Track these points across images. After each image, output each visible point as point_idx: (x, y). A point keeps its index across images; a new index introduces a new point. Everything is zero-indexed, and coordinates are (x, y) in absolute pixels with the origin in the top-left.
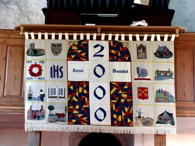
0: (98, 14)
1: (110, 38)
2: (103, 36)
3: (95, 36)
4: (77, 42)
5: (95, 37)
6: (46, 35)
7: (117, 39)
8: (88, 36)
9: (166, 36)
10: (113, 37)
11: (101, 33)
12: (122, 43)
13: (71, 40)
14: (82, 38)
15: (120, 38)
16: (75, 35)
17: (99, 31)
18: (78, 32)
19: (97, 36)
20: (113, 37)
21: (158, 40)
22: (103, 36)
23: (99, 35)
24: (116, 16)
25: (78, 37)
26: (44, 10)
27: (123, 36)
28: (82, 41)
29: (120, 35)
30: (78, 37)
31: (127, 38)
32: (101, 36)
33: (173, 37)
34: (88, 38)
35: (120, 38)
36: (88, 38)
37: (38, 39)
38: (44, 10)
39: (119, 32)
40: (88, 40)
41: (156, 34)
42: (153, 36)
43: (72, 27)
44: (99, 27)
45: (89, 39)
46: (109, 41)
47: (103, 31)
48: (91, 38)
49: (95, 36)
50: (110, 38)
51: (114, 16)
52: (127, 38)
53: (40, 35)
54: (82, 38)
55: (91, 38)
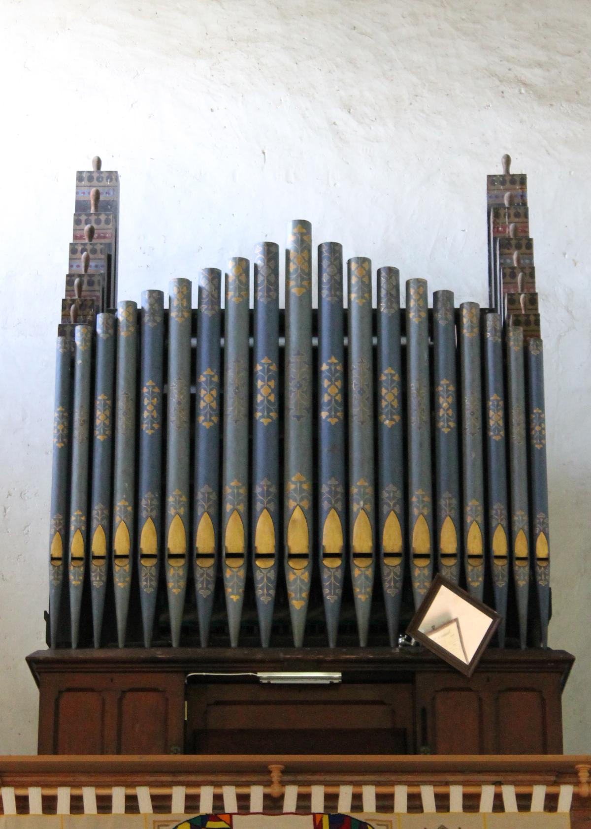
0: (259, 675)
1: (318, 804)
2: (291, 794)
3: (257, 794)
4: (188, 821)
5: (257, 803)
6: (89, 795)
7: (344, 807)
8: (230, 795)
9: (539, 793)
10: (331, 799)
11: (283, 784)
12: (365, 824)
13: (162, 817)
14: (206, 807)
15: (357, 801)
16: (178, 795)
17: (276, 776)
18: (300, 778)
19: (266, 797)
20: (331, 799)
21: (451, 810)
22: (291, 794)
23: (275, 790)
24: (336, 681)
25: (192, 802)
26: (34, 662)
27: (369, 794)
28: (206, 818)
29: (218, 791)
30: (192, 802)
31: (385, 803)
32: (282, 797)
33: (566, 793)
34: (231, 805)
35: (357, 801)
36: (231, 805)
37: (84, 813)
38: (34, 662)
39: (328, 778)
40: (231, 815)
41: (498, 784)
42: (487, 793)
43: (233, 763)
44: (275, 761)
45: (236, 811)
46: (314, 815)
47: (291, 773)
48: (243, 801)
49: (257, 794)
50: (318, 804)
51: (327, 682)
52: (385, 803)
53: (118, 795)
54: (206, 807)
55: (243, 801)
